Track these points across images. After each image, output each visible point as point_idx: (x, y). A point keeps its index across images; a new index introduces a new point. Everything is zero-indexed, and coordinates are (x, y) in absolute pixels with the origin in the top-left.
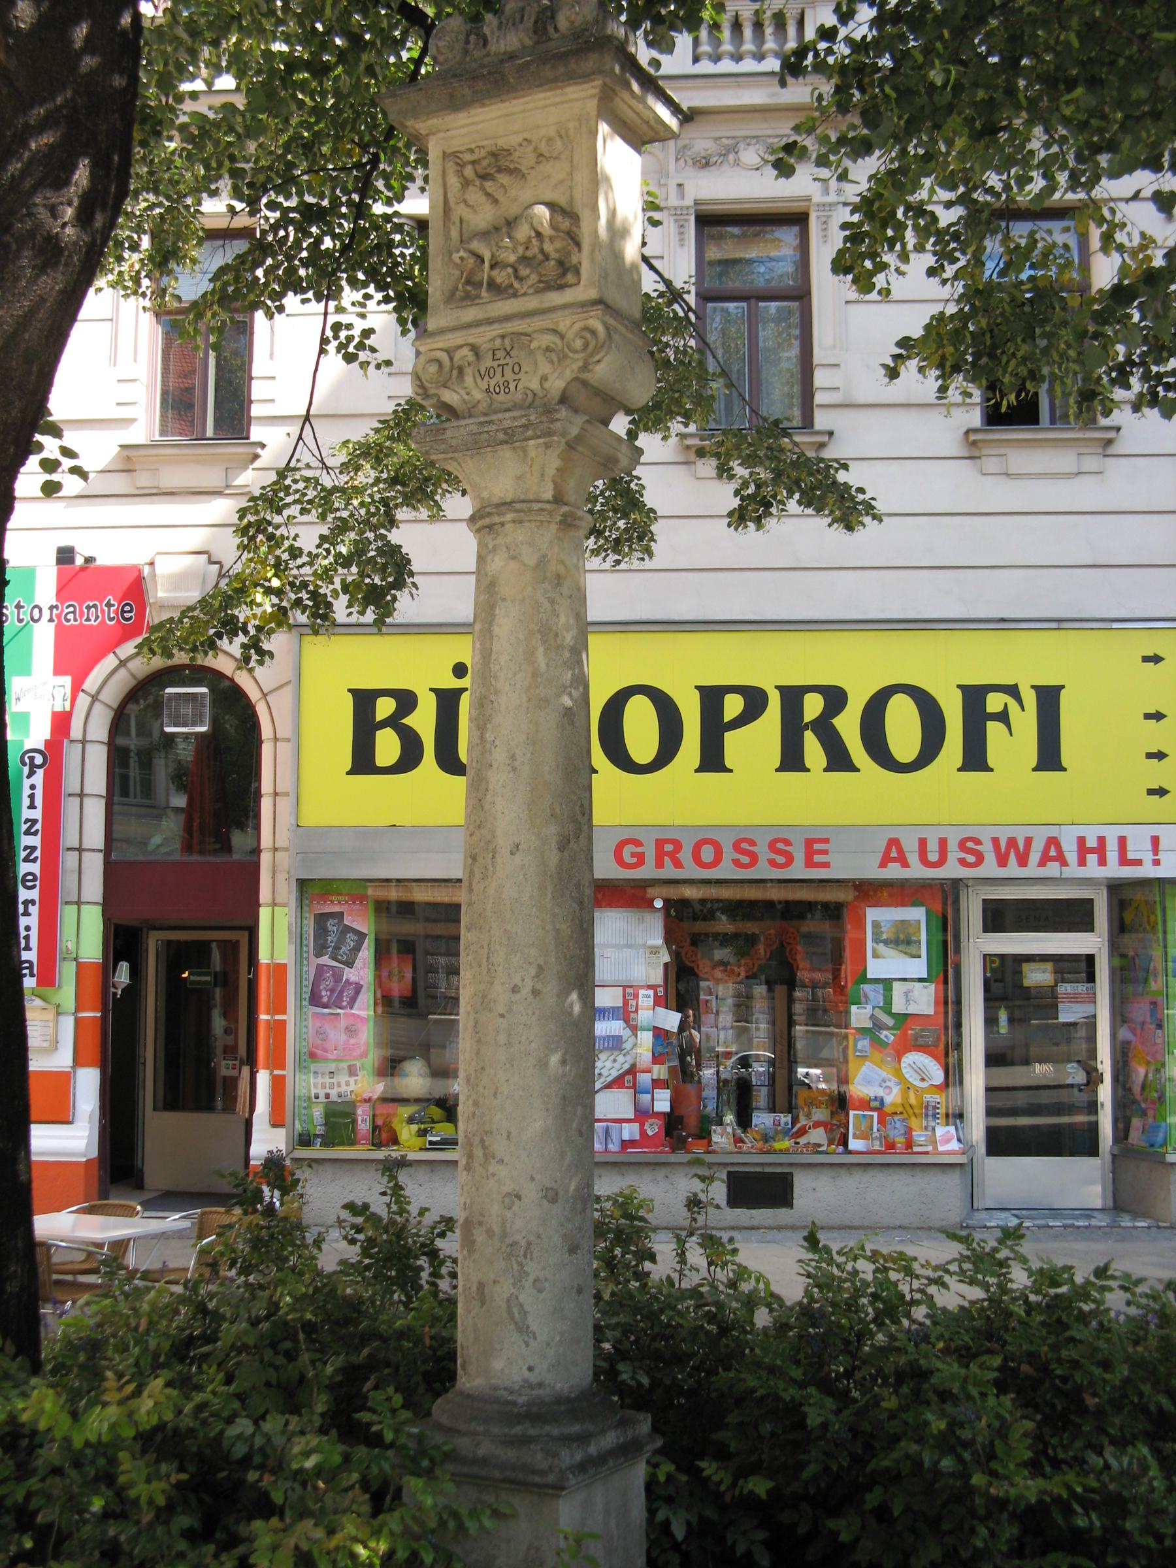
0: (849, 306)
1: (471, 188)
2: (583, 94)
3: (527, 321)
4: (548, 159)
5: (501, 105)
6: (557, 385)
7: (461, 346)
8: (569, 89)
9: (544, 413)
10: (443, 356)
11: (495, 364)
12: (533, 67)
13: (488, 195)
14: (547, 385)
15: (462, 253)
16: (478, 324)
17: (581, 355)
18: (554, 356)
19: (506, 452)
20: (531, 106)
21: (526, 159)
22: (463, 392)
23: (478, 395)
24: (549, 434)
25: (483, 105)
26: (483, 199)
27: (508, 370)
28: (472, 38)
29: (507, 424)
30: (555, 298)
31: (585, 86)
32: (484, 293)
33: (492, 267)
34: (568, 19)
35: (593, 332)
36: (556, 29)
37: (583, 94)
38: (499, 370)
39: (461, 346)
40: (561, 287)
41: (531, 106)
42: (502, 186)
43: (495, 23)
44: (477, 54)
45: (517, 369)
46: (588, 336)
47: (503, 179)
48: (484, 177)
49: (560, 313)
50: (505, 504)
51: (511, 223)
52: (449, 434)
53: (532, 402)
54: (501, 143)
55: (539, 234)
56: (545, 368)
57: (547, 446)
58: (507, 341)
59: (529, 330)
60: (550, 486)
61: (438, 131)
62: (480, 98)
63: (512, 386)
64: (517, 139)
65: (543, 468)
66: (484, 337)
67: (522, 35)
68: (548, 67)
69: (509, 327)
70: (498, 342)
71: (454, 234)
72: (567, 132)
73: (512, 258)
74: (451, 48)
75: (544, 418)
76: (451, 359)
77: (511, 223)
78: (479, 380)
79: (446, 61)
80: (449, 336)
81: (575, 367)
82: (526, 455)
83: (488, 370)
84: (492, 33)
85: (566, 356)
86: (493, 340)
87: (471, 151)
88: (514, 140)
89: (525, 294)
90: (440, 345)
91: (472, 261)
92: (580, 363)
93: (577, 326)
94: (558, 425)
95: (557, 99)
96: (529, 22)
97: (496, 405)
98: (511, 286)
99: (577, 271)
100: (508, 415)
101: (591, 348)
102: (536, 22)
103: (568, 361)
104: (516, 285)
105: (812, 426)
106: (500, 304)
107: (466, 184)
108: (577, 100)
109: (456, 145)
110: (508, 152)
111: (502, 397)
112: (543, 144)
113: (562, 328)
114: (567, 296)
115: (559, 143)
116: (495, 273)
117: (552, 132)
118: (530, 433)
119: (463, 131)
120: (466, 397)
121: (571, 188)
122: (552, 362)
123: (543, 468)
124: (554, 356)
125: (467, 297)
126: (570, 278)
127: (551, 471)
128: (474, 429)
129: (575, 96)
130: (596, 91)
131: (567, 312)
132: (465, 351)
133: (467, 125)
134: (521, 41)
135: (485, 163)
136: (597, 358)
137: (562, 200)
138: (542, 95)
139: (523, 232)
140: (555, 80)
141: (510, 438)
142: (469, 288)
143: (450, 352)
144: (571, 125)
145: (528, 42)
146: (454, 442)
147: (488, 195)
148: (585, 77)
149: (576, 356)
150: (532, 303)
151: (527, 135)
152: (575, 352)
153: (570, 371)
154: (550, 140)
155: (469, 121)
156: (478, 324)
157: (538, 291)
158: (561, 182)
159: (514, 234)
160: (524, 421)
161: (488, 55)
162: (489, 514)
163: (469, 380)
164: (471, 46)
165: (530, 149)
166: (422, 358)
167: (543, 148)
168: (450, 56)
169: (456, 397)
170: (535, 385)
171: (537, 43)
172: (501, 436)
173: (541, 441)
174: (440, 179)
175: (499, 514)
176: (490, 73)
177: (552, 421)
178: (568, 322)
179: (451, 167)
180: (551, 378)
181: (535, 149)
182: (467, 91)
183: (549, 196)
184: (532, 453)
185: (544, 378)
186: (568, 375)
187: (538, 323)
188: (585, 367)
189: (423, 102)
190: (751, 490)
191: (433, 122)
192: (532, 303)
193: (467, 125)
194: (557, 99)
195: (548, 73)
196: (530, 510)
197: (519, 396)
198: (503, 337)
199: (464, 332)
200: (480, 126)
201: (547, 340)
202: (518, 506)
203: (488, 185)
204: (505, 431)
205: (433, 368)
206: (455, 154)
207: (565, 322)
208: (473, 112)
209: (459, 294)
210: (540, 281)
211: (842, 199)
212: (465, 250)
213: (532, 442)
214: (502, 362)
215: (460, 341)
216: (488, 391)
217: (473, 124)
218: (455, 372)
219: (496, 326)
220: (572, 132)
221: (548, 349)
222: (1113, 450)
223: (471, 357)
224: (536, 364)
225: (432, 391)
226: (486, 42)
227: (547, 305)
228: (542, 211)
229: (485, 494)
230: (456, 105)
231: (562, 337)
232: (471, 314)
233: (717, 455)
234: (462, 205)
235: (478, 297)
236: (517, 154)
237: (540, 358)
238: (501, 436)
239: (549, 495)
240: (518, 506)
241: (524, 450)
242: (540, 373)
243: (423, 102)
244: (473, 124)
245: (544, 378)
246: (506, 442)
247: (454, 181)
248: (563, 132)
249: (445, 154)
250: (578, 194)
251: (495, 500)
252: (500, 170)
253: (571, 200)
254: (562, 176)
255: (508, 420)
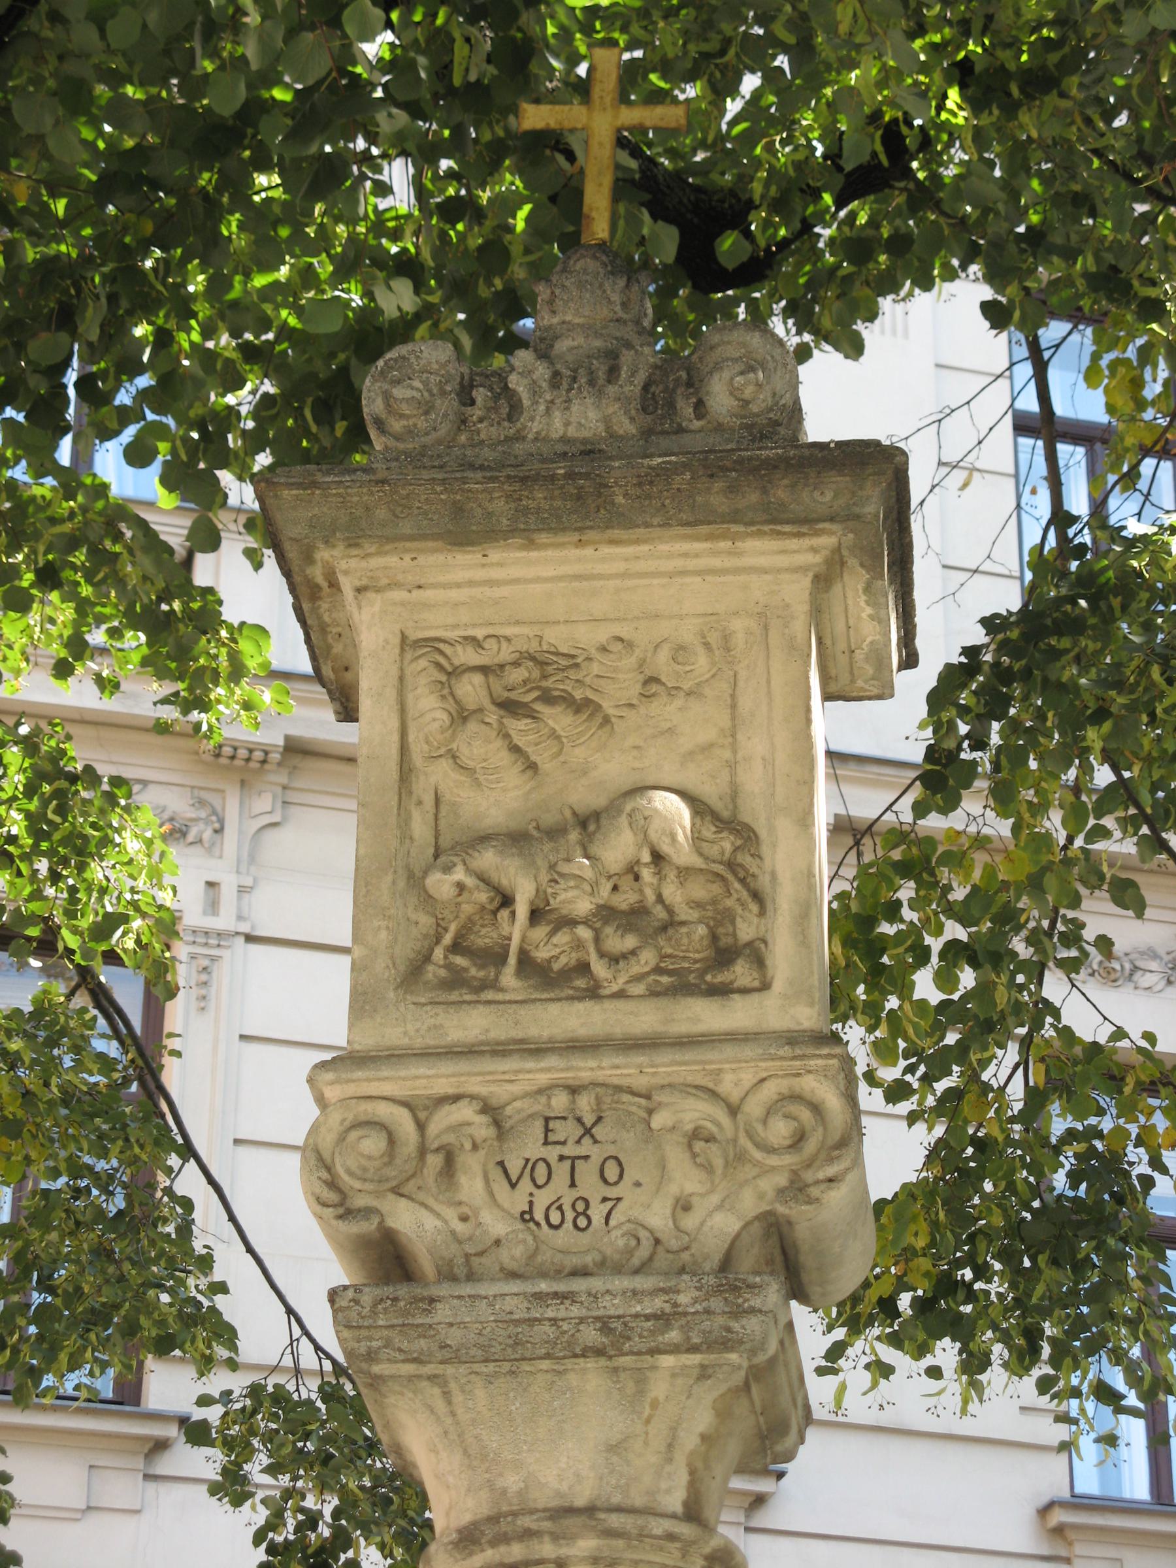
0: (242, 1150)
1: (472, 726)
2: (783, 561)
3: (640, 1059)
4: (673, 691)
5: (574, 553)
6: (720, 1222)
7: (456, 1098)
8: (751, 544)
9: (718, 1290)
10: (403, 1121)
11: (552, 1154)
12: (681, 480)
13: (515, 749)
14: (690, 1222)
15: (459, 874)
16: (500, 1050)
17: (788, 1160)
18: (715, 1155)
19: (590, 1378)
20: (641, 566)
21: (617, 687)
22: (451, 1214)
23: (496, 1225)
24: (726, 1343)
25: (531, 545)
26: (503, 757)
27: (587, 1174)
28: (480, 395)
29: (611, 1306)
30: (705, 1015)
31: (793, 543)
32: (508, 977)
33: (536, 915)
34: (733, 391)
35: (816, 1109)
36: (700, 408)
37: (783, 561)
38: (562, 1172)
39: (456, 1098)
40: (722, 991)
41: (641, 566)
42: (554, 735)
43: (542, 371)
44: (487, 431)
45: (612, 1172)
46: (806, 1115)
47: (557, 719)
48: (510, 707)
49: (730, 1051)
50: (570, 1511)
51: (588, 823)
52: (442, 1313)
53: (649, 1257)
54: (557, 638)
55: (658, 858)
56: (685, 1179)
57: (704, 1374)
58: (585, 1103)
59: (641, 1082)
60: (683, 1477)
61: (394, 585)
62: (524, 528)
63: (597, 1213)
64: (602, 634)
65: (674, 1430)
66: (515, 1082)
67: (613, 408)
68: (718, 485)
69: (586, 1068)
70: (560, 1101)
71: (420, 828)
72: (726, 638)
73: (583, 906)
74: (428, 409)
75: (716, 1304)
76: (421, 1126)
77: (588, 823)
78: (501, 1187)
79: (410, 432)
80: (421, 1069)
81: (769, 1184)
82: (641, 1392)
83: (530, 1166)
84: (535, 391)
85: (742, 1157)
86: (544, 1091)
87: (473, 641)
88: (588, 637)
89: (620, 995)
90: (387, 1089)
91: (483, 897)
92: (782, 1180)
93: (770, 1090)
94: (753, 1324)
95: (716, 562)
96: (631, 385)
97: (545, 1257)
98: (583, 968)
99: (756, 954)
100: (620, 1283)
101: (811, 1146)
102: (646, 388)
103: (748, 1171)
104: (599, 968)
105: (136, 1399)
106: (554, 1009)
107: (462, 716)
108: (764, 571)
109: (435, 624)
110: (572, 662)
111: (565, 1237)
112: (664, 655)
113: (729, 1086)
114: (736, 1014)
115: (702, 662)
116: (540, 932)
117: (687, 633)
118: (674, 1336)
119: (454, 594)
120: (459, 1227)
121: (732, 766)
122: (708, 1168)
123: (674, 1430)
124: (715, 1155)
125: (455, 981)
126: (741, 973)
127: (689, 1441)
128: (518, 1308)
129: (762, 561)
130: (818, 559)
131: (749, 1051)
132: (465, 1112)
133: (471, 583)
134: (607, 420)
135: (516, 675)
136: (830, 1171)
137: (711, 792)
138: (686, 546)
139: (619, 847)
140: (734, 517)
141: (613, 1341)
142: (460, 961)
143: (420, 1109)
144: (738, 625)
145: (626, 426)
146: (454, 1337)
147: (515, 749)
148: (807, 523)
149: (773, 1161)
150: (644, 1018)
151: (624, 631)
152: (771, 1150)
153: (754, 1197)
154: (680, 651)
155: (480, 574)
156: (500, 1050)
157: (654, 993)
158: (707, 748)
159: (594, 849)
160: (658, 1304)
161: (519, 437)
162: (528, 1534)
163: (471, 1186)
164: (477, 412)
165: (630, 661)
166: (335, 1118)
167: (662, 662)
168: (422, 423)
169: (431, 1223)
170: (658, 1218)
171: (647, 433)
172: (591, 1335)
173: (695, 1359)
174: (391, 694)
175: (556, 1537)
176: (570, 476)
177: (738, 1313)
178: (748, 1077)
179: (422, 670)
180: (700, 1209)
181: (642, 663)
182: (499, 505)
183: (692, 779)
184: (659, 1388)
185: (684, 1205)
186: (750, 1204)
187: (664, 1067)
188: (797, 1189)
189: (381, 513)
190: (288, 1532)
191: (390, 562)
192: (644, 1018)
193: (471, 583)
194: (716, 562)
195: (716, 498)
196: (642, 1536)
197: (617, 1240)
198: (574, 1090)
199: (463, 1066)
200: (504, 591)
201: (695, 1111)
202: (615, 1521)
203: (518, 727)
204: (604, 1323)
205: (373, 1144)
206: (432, 644)
207: (736, 1075)
208: (495, 556)
209: (433, 972)
210: (658, 970)
211: (245, 928)
212: (469, 871)
213: (667, 1361)
214: (570, 1150)
215: (443, 1087)
216: (527, 1216)
217: (491, 583)
218: (434, 1161)
219: (552, 1061)
220: (739, 640)
221: (696, 1135)
222: (763, 1519)
223: (482, 1128)
224: (662, 1166)
225: (360, 1202)
226: (515, 409)
227: (681, 1028)
228: (672, 809)
229: (512, 1482)
230: (463, 531)
231: (733, 1111)
232: (472, 1023)
233: (229, 1444)
234: (445, 765)
235: (494, 985)
236: (595, 668)
237: (676, 1156)
238: (591, 1335)
239: (675, 1501)
240: (615, 1521)
241: (641, 1379)
242: (673, 1189)
243: (381, 513)
244: (491, 583)
245: (684, 1205)
246: (599, 1352)
247: (429, 708)
248: (714, 638)
249: (405, 643)
250: (752, 780)
251: (542, 1499)
252: (547, 698)
253: (734, 794)
254: (707, 735)
255: (614, 1295)
